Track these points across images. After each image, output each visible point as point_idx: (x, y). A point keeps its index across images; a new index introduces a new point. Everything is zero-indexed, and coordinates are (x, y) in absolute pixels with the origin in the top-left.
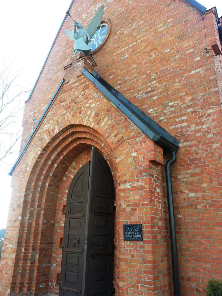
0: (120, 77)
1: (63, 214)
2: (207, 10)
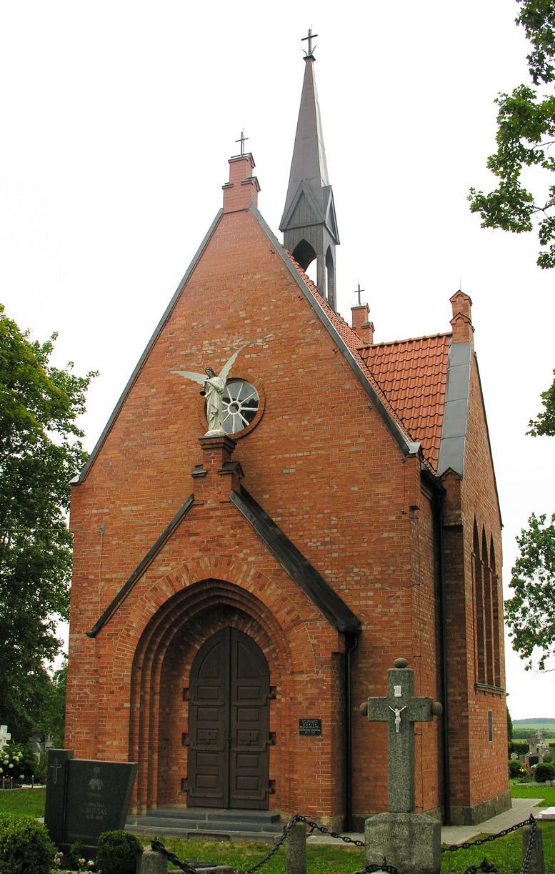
0: (281, 502)
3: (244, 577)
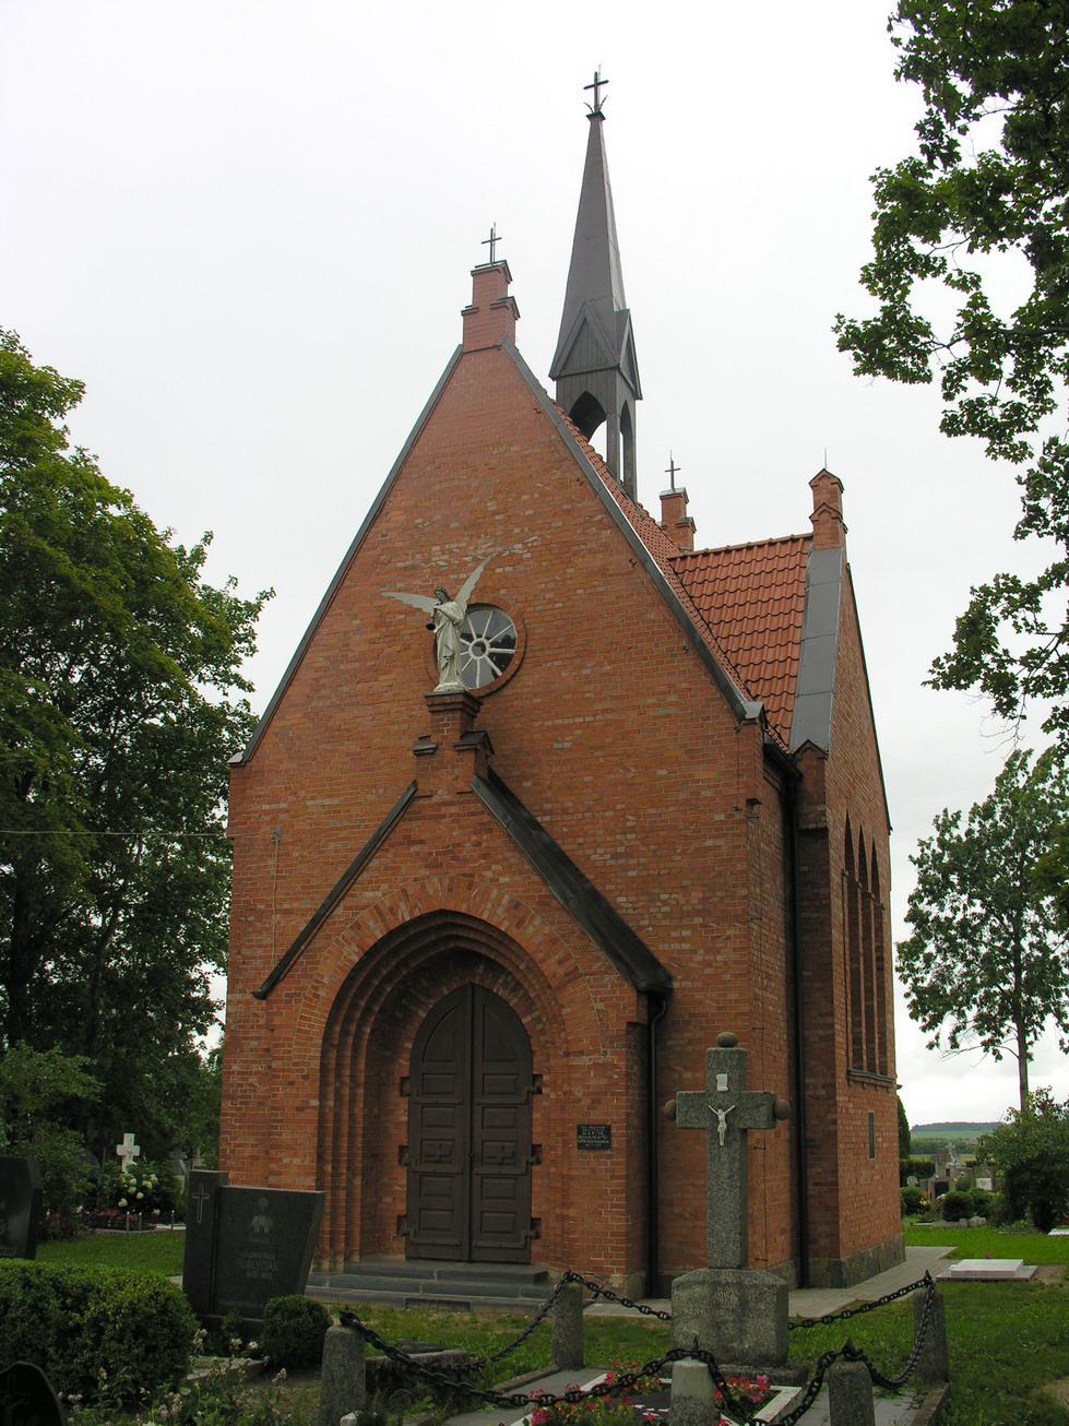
1: (401, 1095)
2: (747, 717)
3: (493, 908)
